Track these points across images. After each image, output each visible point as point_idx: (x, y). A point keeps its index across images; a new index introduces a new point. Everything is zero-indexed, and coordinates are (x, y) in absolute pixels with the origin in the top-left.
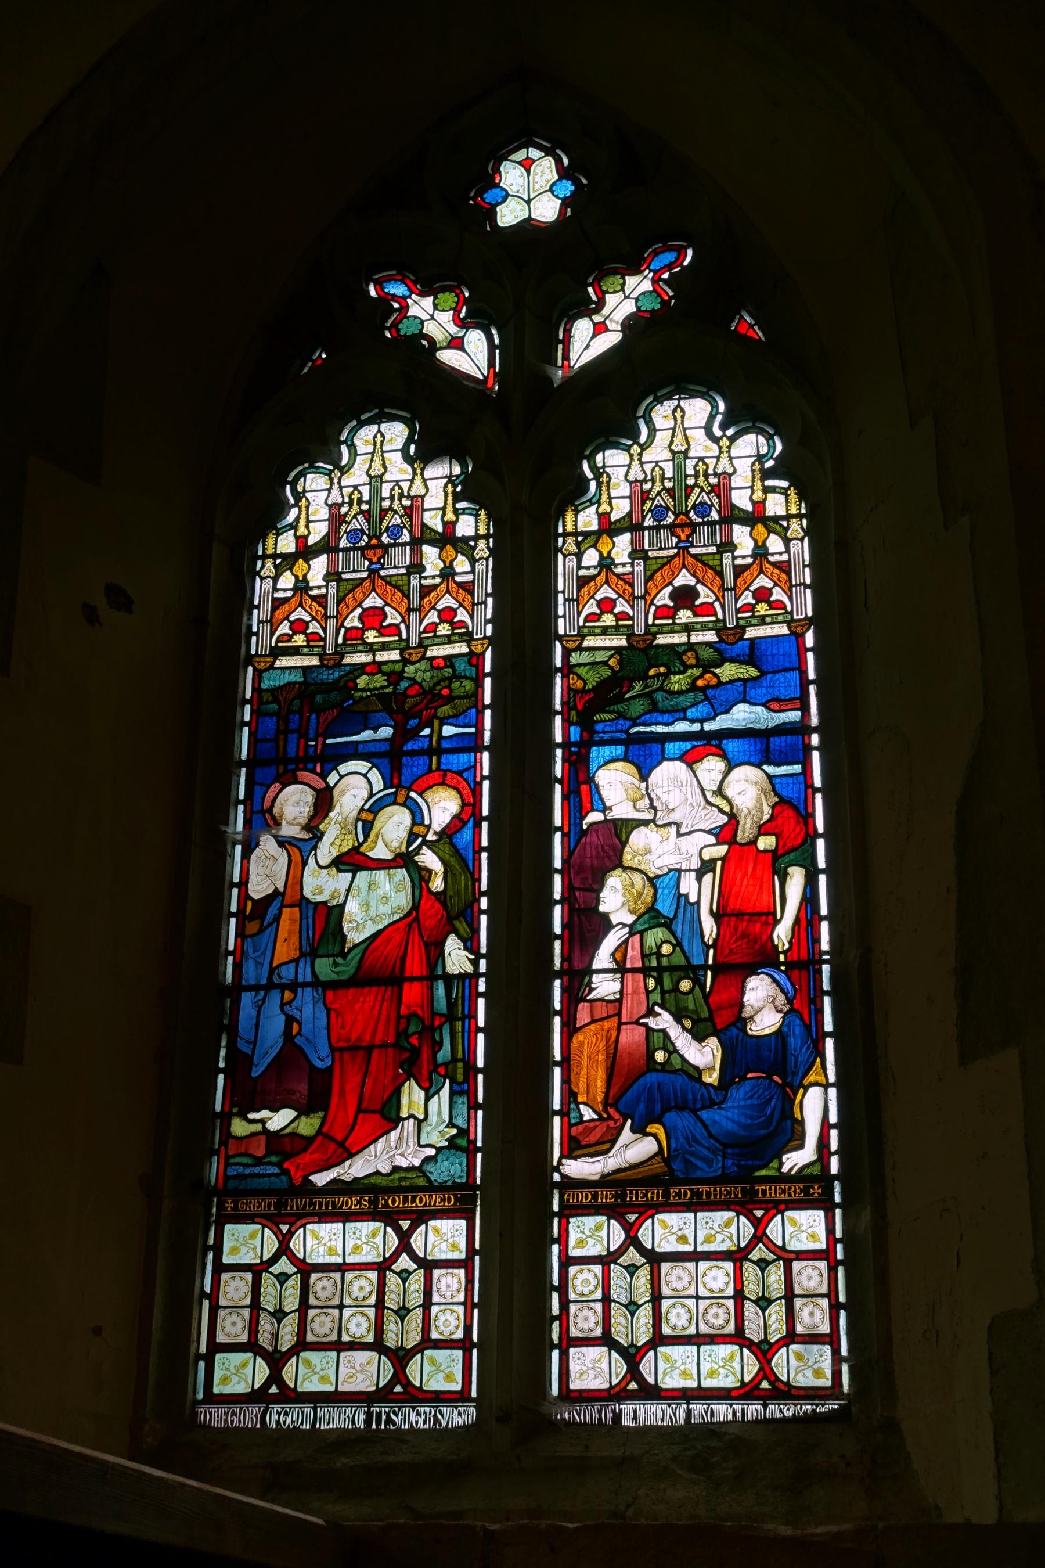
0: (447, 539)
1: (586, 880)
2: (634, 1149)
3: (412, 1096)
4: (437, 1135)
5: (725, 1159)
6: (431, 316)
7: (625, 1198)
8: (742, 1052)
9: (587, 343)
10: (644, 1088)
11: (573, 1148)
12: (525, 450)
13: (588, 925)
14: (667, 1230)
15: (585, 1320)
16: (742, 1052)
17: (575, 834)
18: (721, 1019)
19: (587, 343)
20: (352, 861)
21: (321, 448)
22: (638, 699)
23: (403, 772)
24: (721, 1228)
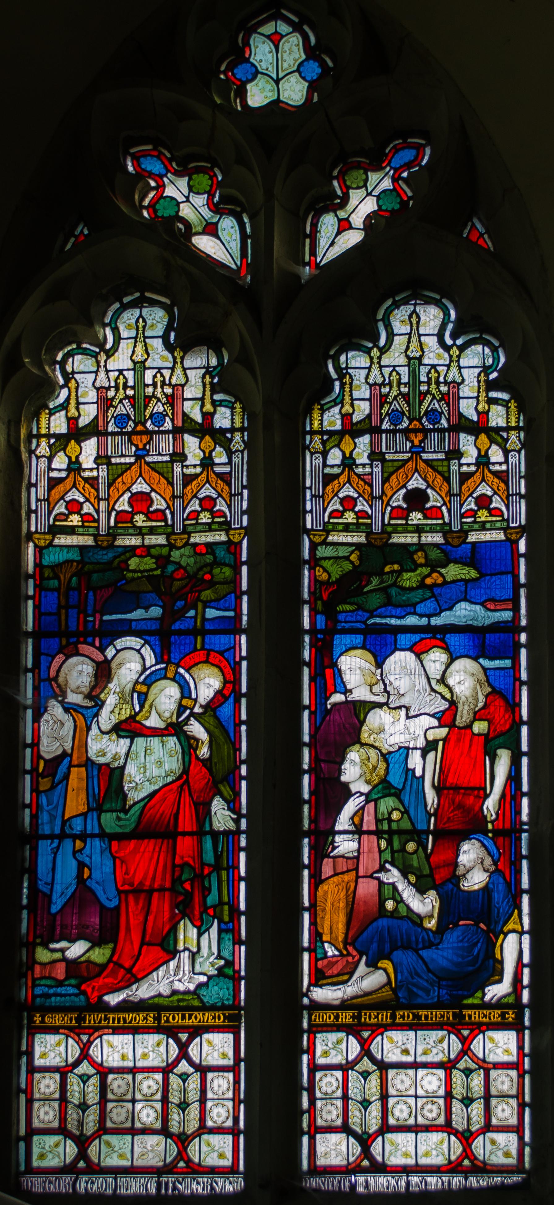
0: (479, 428)
1: (330, 756)
2: (368, 980)
3: (187, 934)
4: (208, 964)
5: (440, 987)
6: (185, 198)
7: (361, 1019)
8: (457, 905)
9: (336, 239)
10: (376, 932)
11: (319, 978)
12: (278, 343)
13: (332, 793)
14: (392, 1045)
15: (329, 1113)
16: (457, 905)
17: (322, 714)
18: (438, 876)
19: (336, 239)
20: (129, 728)
21: (79, 323)
22: (376, 596)
23: (175, 647)
24: (437, 1044)
